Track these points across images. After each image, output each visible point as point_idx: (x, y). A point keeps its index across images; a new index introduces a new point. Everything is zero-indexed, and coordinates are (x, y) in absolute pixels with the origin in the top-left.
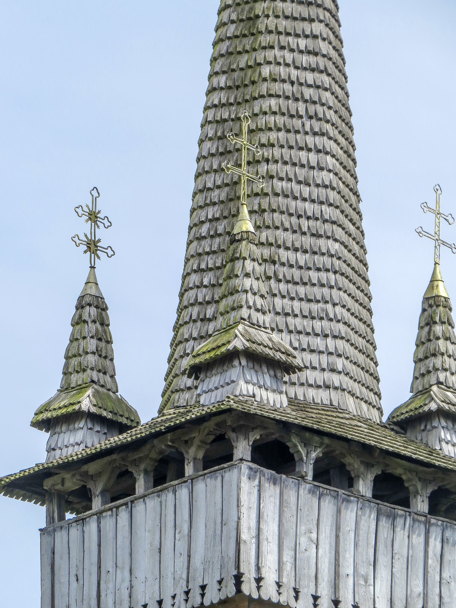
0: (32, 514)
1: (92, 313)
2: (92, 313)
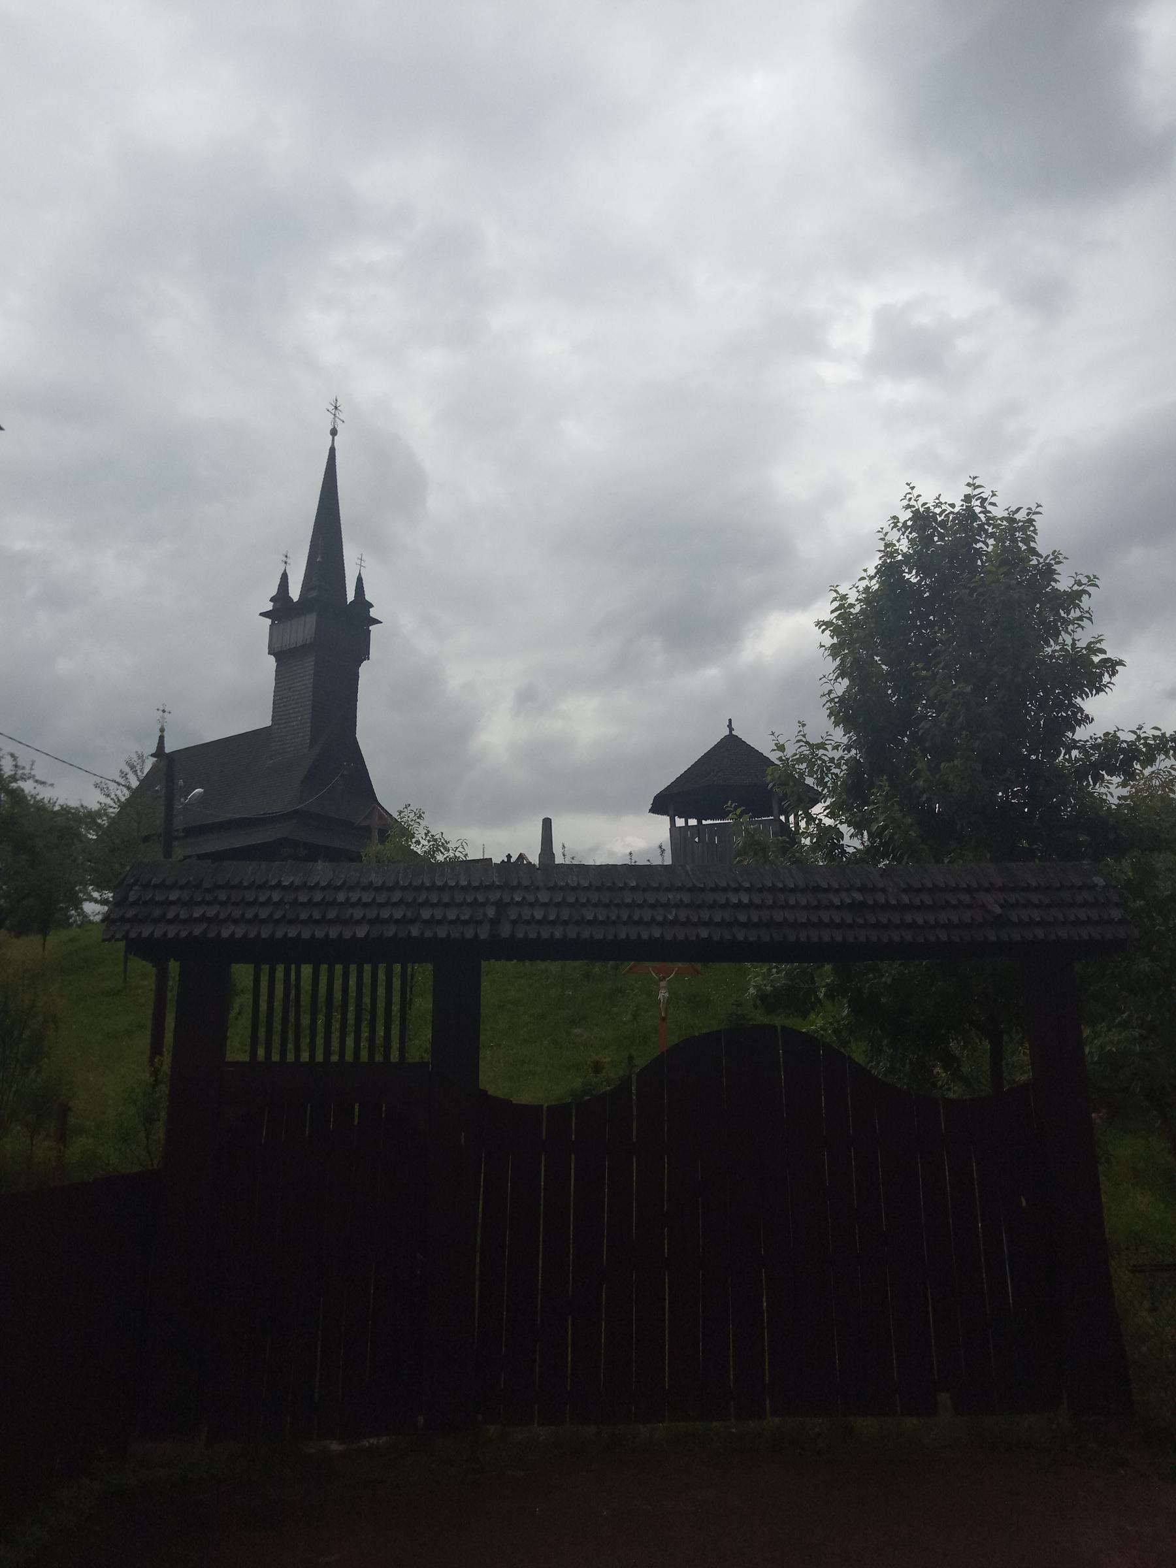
0: (269, 621)
1: (284, 578)
2: (284, 578)
